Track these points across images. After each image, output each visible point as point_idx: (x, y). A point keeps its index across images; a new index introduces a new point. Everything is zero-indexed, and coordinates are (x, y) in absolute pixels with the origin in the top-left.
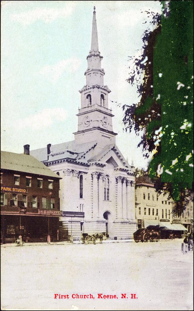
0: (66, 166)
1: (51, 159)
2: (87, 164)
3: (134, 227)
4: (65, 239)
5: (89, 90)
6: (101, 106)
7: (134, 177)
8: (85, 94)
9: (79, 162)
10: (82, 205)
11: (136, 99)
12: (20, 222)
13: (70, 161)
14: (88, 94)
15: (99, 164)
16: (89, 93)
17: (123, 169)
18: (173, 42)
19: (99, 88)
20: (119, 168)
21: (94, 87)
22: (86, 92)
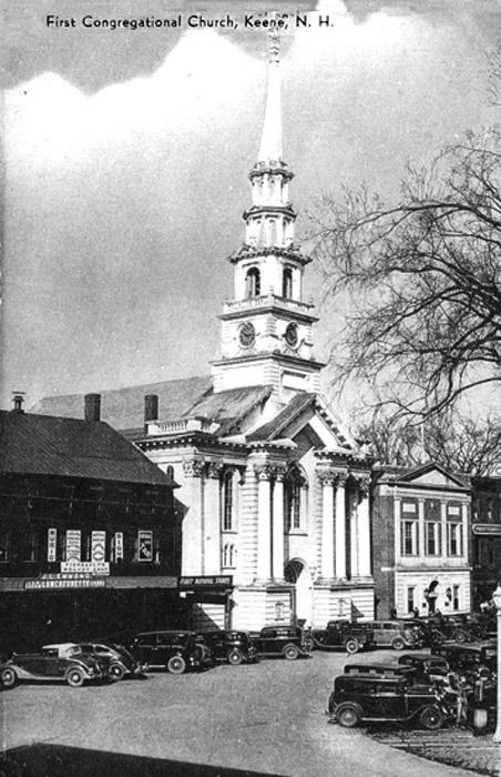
0: (189, 452)
1: (153, 430)
2: (244, 446)
3: (67, 580)
4: (388, 691)
5: (255, 259)
6: (284, 298)
7: (428, 458)
8: (244, 266)
9: (224, 444)
10: (229, 548)
11: (177, 493)
12: (384, 720)
13: (203, 441)
14: (252, 266)
15: (274, 446)
16: (257, 266)
17: (338, 454)
18: (50, 622)
19: (278, 255)
20: (327, 450)
21: (266, 253)
22: (245, 262)
